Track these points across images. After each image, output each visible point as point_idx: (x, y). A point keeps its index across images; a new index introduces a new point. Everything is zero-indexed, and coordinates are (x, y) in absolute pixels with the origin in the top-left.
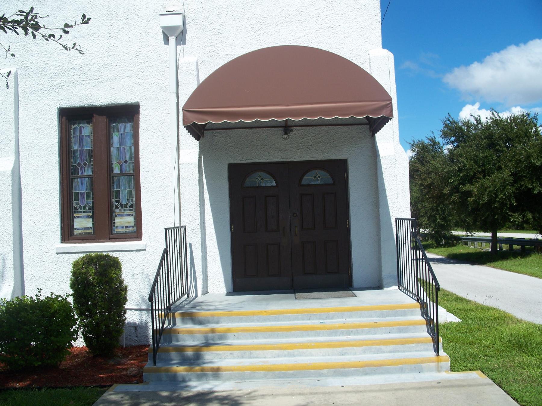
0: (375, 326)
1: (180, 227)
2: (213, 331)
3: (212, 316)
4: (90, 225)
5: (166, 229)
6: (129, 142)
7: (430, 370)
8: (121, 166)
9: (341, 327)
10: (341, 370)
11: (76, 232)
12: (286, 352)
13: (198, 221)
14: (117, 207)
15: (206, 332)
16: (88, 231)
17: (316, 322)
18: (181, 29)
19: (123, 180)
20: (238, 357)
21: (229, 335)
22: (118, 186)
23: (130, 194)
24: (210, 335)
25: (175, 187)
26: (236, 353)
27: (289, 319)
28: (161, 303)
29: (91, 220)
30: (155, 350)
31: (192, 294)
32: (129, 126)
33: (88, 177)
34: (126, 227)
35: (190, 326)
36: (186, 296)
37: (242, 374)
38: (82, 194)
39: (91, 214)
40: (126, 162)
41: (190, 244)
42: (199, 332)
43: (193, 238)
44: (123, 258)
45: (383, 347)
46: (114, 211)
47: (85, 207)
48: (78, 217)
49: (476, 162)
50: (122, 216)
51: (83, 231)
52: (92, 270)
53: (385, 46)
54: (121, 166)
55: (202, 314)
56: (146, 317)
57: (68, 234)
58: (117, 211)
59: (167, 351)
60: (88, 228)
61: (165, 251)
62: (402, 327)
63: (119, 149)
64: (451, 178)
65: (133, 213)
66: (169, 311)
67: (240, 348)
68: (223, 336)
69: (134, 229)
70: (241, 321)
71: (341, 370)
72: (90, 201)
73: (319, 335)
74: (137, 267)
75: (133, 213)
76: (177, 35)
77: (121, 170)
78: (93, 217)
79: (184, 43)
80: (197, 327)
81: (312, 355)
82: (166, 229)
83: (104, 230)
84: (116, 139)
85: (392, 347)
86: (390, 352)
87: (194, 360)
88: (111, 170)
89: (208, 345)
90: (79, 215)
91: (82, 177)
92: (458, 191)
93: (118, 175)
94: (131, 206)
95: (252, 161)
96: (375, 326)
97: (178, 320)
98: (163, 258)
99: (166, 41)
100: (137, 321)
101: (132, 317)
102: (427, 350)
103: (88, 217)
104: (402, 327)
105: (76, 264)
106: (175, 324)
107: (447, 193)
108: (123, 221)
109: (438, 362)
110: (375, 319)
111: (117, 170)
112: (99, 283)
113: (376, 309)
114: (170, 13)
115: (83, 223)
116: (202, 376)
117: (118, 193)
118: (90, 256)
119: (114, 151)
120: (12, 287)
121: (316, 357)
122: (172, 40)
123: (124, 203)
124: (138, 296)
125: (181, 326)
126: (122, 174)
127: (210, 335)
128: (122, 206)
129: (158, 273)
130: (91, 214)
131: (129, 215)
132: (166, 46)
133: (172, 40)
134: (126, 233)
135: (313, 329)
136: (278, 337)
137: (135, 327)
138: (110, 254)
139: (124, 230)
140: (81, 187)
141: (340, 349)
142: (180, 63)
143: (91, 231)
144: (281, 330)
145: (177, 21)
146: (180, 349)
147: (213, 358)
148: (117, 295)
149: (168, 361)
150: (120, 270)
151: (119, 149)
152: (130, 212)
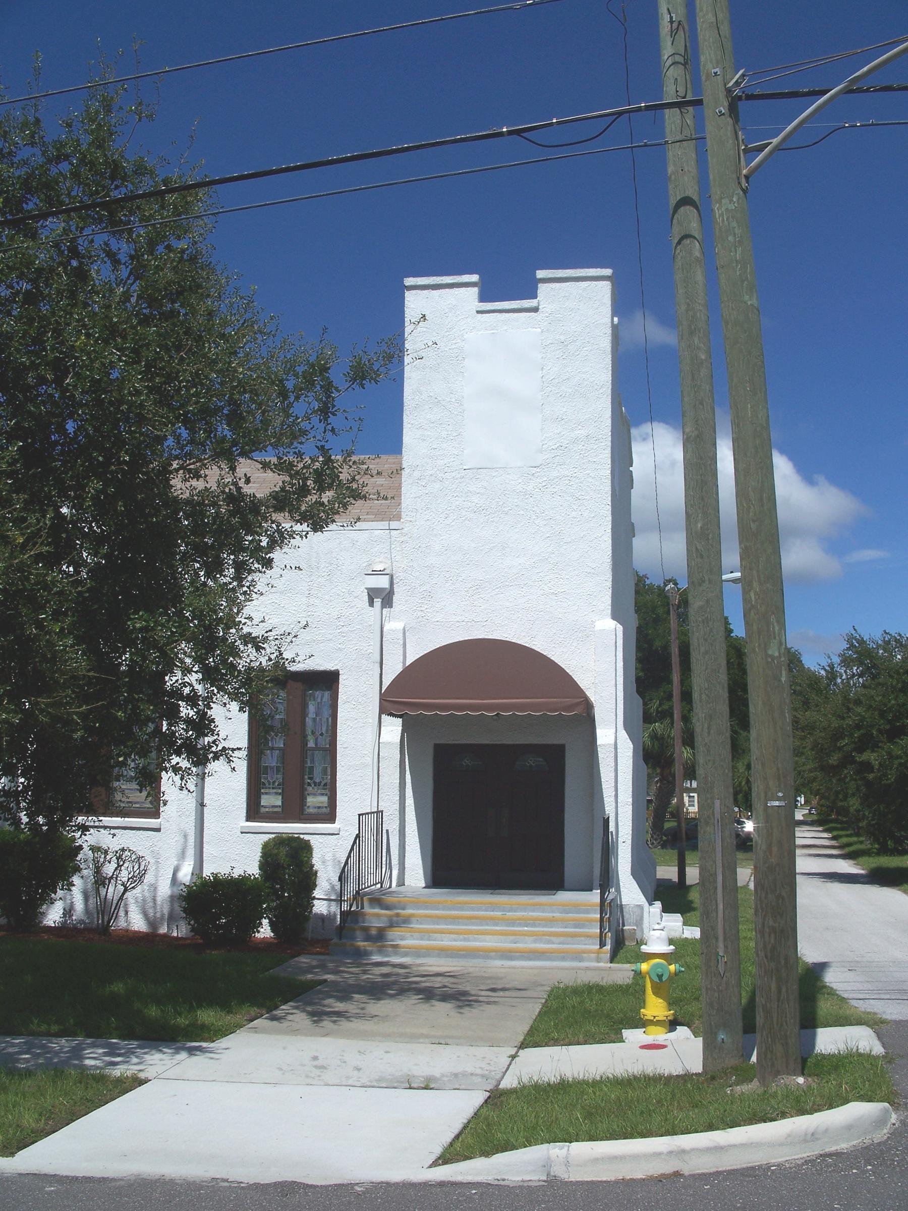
0: (551, 921)
1: (377, 812)
2: (398, 915)
3: (399, 902)
4: (279, 803)
5: (359, 815)
6: (326, 713)
7: (590, 960)
8: (316, 739)
9: (519, 919)
10: (507, 954)
11: (263, 810)
12: (461, 936)
13: (397, 806)
14: (309, 784)
15: (391, 916)
16: (276, 810)
17: (498, 914)
18: (387, 591)
19: (318, 755)
20: (417, 939)
21: (413, 919)
22: (313, 761)
23: (325, 772)
24: (395, 919)
25: (372, 760)
26: (416, 935)
27: (473, 909)
28: (351, 888)
29: (280, 797)
30: (341, 928)
31: (386, 884)
32: (327, 694)
33: (279, 749)
34: (319, 807)
35: (377, 910)
36: (379, 886)
37: (418, 952)
38: (272, 768)
39: (280, 791)
40: (322, 734)
41: (387, 831)
42: (385, 915)
43: (391, 824)
44: (314, 841)
45: (553, 938)
46: (306, 790)
47: (274, 783)
48: (266, 793)
49: (882, 715)
50: (315, 795)
51: (271, 810)
52: (283, 851)
53: (615, 617)
54: (316, 739)
55: (389, 899)
56: (334, 908)
57: (254, 812)
58: (310, 789)
59: (354, 930)
60: (276, 807)
61: (358, 836)
62: (578, 924)
63: (314, 720)
64: (843, 739)
65: (327, 792)
66: (358, 895)
67: (420, 931)
68: (407, 920)
69: (327, 811)
70: (426, 908)
71: (507, 954)
72: (280, 776)
73: (497, 925)
74: (328, 850)
75: (327, 792)
76: (383, 597)
77: (316, 744)
78: (282, 794)
79: (391, 607)
80: (383, 912)
81: (486, 941)
82: (359, 815)
83: (294, 810)
84: (311, 708)
85: (562, 939)
86: (560, 943)
87: (379, 937)
88: (305, 742)
89: (391, 925)
90: (267, 791)
91: (272, 749)
92: (853, 761)
93: (313, 749)
94: (325, 785)
95: (459, 742)
96: (551, 921)
97: (366, 904)
98: (355, 842)
99: (371, 603)
100: (325, 912)
101: (320, 907)
102: (594, 944)
103: (276, 793)
104: (578, 924)
105: (266, 846)
106: (362, 908)
107: (835, 763)
108: (316, 801)
109: (598, 953)
110: (551, 915)
111: (311, 744)
112: (288, 865)
113: (559, 905)
114: (375, 573)
115: (271, 800)
116: (381, 951)
117: (311, 769)
118: (282, 837)
119: (309, 721)
120: (192, 866)
121: (489, 942)
122: (378, 602)
123: (317, 781)
124: (327, 884)
125: (368, 909)
126: (317, 748)
127: (395, 919)
128: (315, 783)
129: (349, 856)
130: (280, 791)
131: (323, 794)
132: (371, 608)
133: (378, 602)
134: (318, 814)
135: (492, 919)
136: (458, 924)
137: (322, 918)
138: (302, 836)
139: (315, 811)
140: (271, 760)
141: (512, 938)
142: (385, 629)
143: (280, 810)
144: (462, 917)
145: (383, 582)
146: (366, 929)
147: (394, 935)
148: (306, 880)
149: (353, 938)
150: (311, 853)
151: (314, 720)
152: (324, 791)
